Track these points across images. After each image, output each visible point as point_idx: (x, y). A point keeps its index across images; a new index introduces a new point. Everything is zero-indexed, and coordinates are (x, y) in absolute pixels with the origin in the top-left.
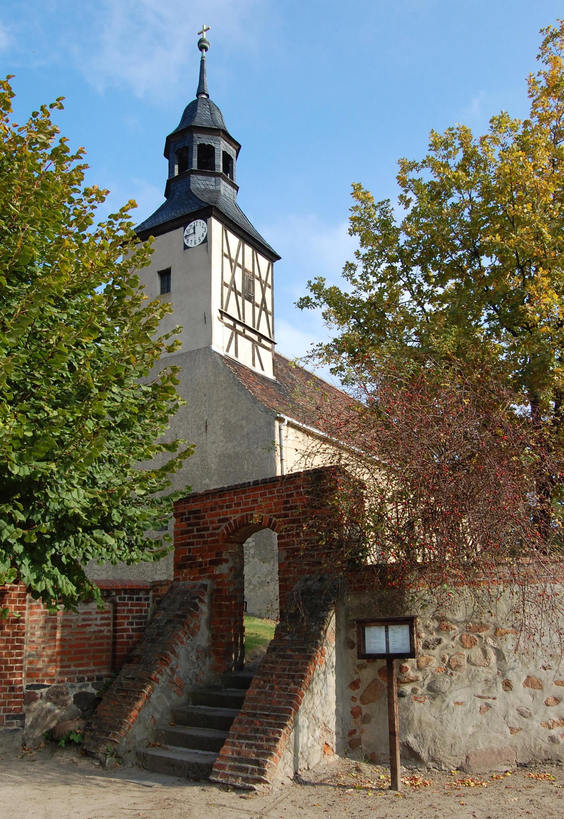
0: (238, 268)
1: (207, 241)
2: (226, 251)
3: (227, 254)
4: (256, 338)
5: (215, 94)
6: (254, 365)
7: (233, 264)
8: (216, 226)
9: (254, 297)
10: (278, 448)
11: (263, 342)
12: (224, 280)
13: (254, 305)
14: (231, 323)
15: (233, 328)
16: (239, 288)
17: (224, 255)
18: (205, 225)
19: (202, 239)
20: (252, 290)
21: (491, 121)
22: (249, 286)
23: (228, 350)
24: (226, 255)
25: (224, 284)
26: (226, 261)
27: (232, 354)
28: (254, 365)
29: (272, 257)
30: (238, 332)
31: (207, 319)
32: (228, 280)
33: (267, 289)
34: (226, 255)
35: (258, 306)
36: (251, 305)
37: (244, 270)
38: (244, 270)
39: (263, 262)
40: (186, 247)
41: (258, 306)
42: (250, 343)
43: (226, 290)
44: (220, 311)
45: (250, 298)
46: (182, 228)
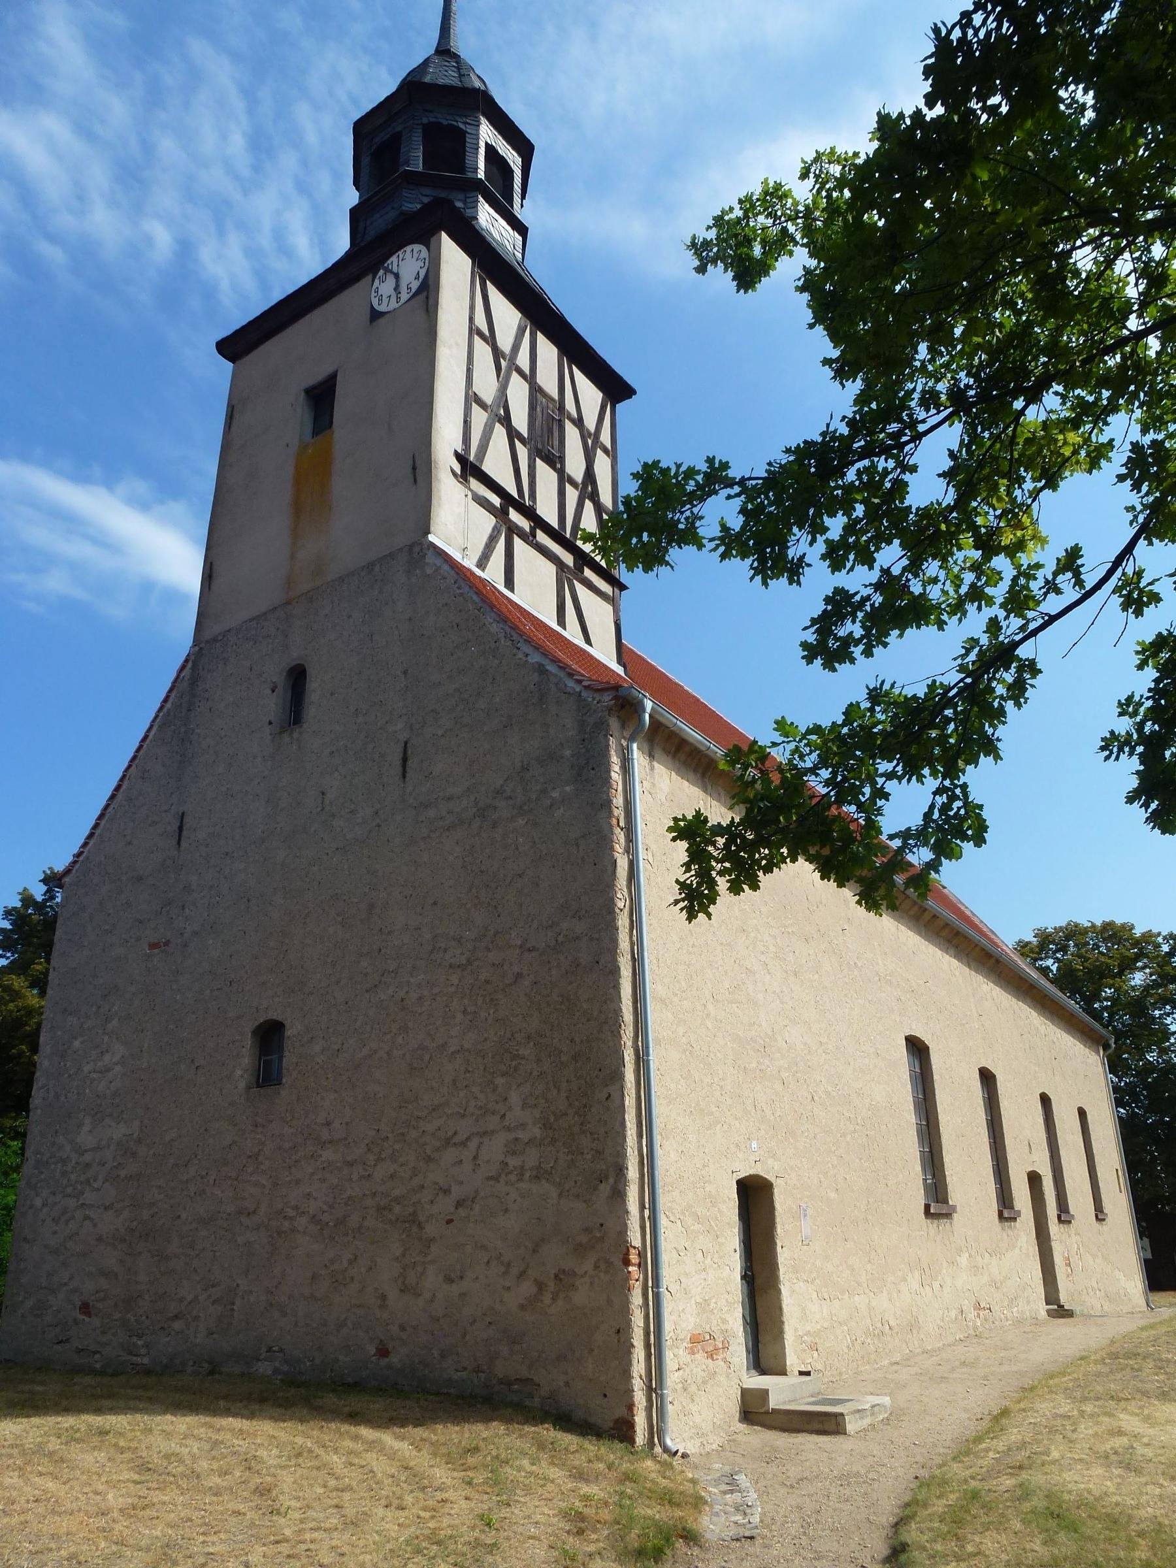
0: (515, 376)
1: (428, 289)
2: (481, 322)
3: (485, 329)
4: (568, 559)
5: (464, 43)
6: (561, 621)
7: (503, 363)
8: (455, 263)
9: (562, 459)
10: (620, 836)
11: (588, 573)
12: (476, 388)
13: (564, 479)
14: (496, 500)
15: (501, 514)
16: (520, 422)
17: (473, 331)
18: (425, 253)
19: (415, 285)
20: (556, 443)
21: (770, 464)
22: (550, 431)
23: (482, 562)
24: (480, 334)
25: (472, 399)
26: (483, 351)
27: (494, 574)
28: (561, 621)
29: (615, 389)
30: (513, 530)
31: (419, 470)
32: (488, 392)
33: (579, 477)
34: (480, 334)
35: (574, 484)
36: (554, 476)
37: (536, 391)
38: (536, 391)
39: (590, 395)
40: (375, 315)
41: (574, 484)
42: (551, 569)
43: (479, 417)
44: (458, 456)
45: (556, 461)
46: (370, 277)
